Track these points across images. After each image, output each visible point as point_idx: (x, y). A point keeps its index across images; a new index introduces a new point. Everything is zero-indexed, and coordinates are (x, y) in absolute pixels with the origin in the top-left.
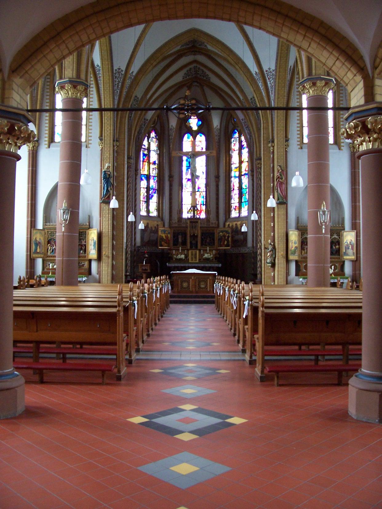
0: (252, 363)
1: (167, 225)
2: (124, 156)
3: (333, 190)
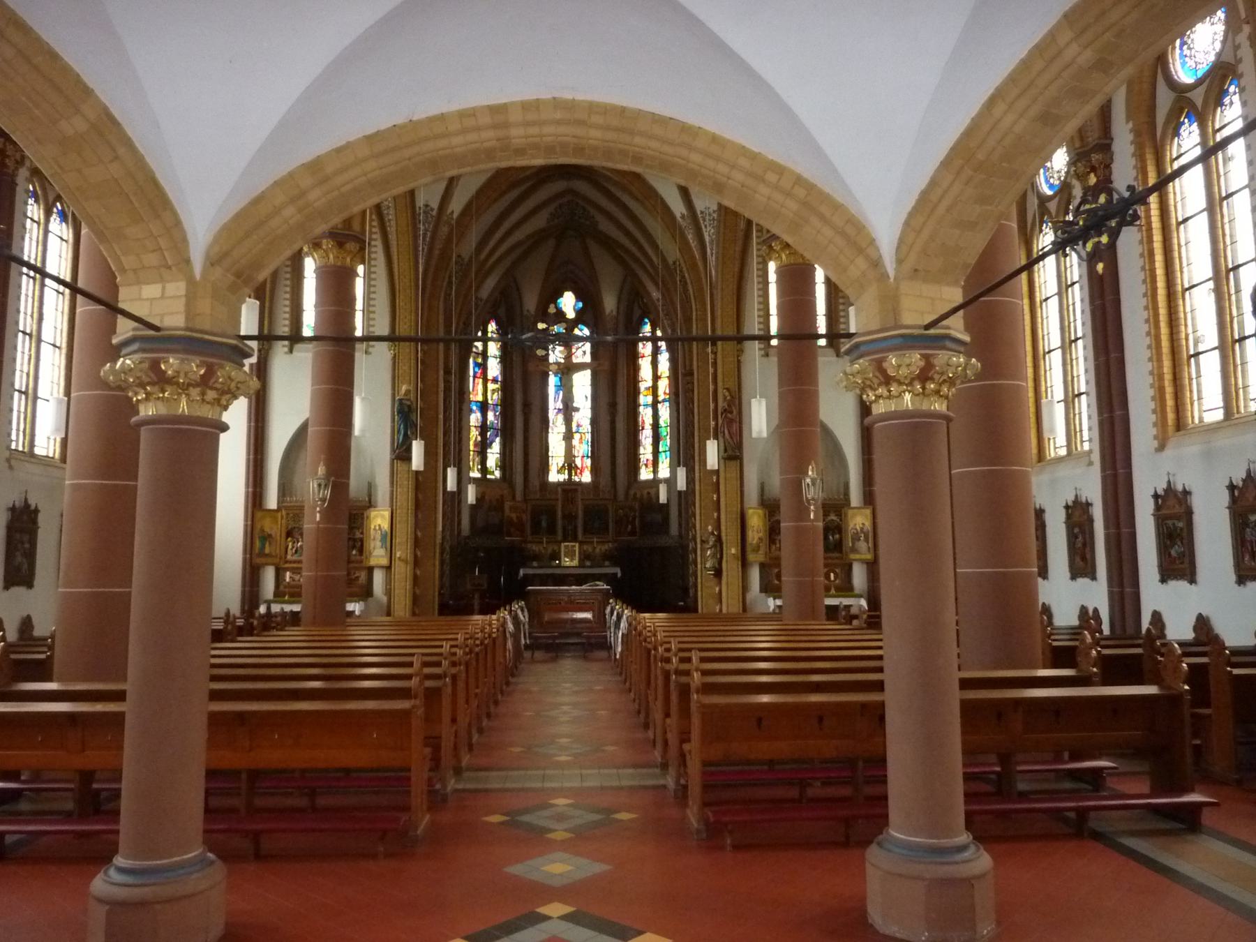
0: (682, 793)
1: (519, 496)
2: (438, 371)
3: (827, 433)
